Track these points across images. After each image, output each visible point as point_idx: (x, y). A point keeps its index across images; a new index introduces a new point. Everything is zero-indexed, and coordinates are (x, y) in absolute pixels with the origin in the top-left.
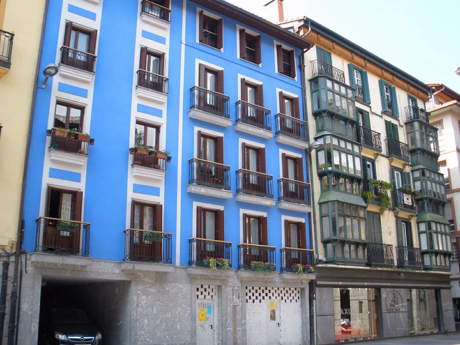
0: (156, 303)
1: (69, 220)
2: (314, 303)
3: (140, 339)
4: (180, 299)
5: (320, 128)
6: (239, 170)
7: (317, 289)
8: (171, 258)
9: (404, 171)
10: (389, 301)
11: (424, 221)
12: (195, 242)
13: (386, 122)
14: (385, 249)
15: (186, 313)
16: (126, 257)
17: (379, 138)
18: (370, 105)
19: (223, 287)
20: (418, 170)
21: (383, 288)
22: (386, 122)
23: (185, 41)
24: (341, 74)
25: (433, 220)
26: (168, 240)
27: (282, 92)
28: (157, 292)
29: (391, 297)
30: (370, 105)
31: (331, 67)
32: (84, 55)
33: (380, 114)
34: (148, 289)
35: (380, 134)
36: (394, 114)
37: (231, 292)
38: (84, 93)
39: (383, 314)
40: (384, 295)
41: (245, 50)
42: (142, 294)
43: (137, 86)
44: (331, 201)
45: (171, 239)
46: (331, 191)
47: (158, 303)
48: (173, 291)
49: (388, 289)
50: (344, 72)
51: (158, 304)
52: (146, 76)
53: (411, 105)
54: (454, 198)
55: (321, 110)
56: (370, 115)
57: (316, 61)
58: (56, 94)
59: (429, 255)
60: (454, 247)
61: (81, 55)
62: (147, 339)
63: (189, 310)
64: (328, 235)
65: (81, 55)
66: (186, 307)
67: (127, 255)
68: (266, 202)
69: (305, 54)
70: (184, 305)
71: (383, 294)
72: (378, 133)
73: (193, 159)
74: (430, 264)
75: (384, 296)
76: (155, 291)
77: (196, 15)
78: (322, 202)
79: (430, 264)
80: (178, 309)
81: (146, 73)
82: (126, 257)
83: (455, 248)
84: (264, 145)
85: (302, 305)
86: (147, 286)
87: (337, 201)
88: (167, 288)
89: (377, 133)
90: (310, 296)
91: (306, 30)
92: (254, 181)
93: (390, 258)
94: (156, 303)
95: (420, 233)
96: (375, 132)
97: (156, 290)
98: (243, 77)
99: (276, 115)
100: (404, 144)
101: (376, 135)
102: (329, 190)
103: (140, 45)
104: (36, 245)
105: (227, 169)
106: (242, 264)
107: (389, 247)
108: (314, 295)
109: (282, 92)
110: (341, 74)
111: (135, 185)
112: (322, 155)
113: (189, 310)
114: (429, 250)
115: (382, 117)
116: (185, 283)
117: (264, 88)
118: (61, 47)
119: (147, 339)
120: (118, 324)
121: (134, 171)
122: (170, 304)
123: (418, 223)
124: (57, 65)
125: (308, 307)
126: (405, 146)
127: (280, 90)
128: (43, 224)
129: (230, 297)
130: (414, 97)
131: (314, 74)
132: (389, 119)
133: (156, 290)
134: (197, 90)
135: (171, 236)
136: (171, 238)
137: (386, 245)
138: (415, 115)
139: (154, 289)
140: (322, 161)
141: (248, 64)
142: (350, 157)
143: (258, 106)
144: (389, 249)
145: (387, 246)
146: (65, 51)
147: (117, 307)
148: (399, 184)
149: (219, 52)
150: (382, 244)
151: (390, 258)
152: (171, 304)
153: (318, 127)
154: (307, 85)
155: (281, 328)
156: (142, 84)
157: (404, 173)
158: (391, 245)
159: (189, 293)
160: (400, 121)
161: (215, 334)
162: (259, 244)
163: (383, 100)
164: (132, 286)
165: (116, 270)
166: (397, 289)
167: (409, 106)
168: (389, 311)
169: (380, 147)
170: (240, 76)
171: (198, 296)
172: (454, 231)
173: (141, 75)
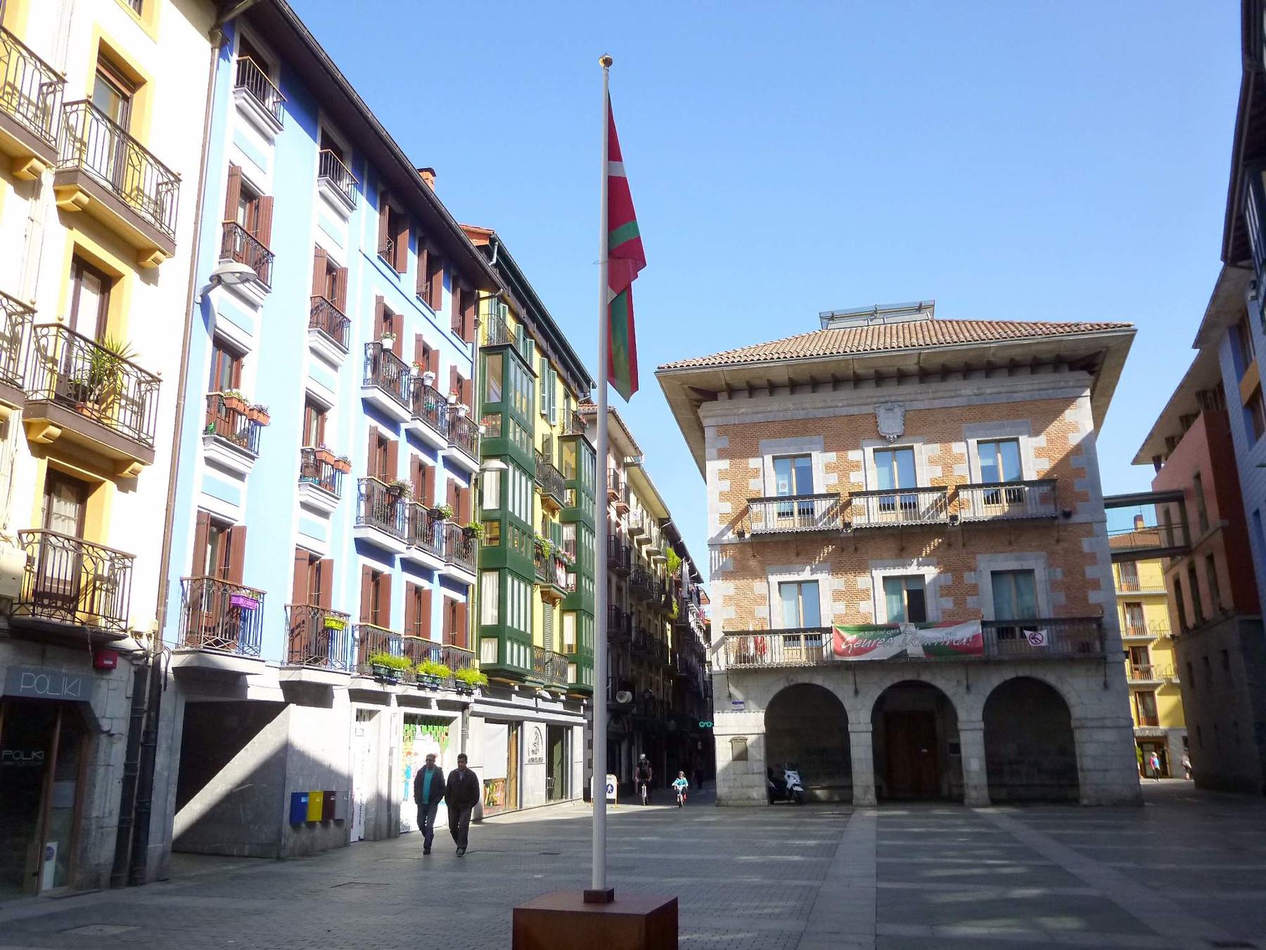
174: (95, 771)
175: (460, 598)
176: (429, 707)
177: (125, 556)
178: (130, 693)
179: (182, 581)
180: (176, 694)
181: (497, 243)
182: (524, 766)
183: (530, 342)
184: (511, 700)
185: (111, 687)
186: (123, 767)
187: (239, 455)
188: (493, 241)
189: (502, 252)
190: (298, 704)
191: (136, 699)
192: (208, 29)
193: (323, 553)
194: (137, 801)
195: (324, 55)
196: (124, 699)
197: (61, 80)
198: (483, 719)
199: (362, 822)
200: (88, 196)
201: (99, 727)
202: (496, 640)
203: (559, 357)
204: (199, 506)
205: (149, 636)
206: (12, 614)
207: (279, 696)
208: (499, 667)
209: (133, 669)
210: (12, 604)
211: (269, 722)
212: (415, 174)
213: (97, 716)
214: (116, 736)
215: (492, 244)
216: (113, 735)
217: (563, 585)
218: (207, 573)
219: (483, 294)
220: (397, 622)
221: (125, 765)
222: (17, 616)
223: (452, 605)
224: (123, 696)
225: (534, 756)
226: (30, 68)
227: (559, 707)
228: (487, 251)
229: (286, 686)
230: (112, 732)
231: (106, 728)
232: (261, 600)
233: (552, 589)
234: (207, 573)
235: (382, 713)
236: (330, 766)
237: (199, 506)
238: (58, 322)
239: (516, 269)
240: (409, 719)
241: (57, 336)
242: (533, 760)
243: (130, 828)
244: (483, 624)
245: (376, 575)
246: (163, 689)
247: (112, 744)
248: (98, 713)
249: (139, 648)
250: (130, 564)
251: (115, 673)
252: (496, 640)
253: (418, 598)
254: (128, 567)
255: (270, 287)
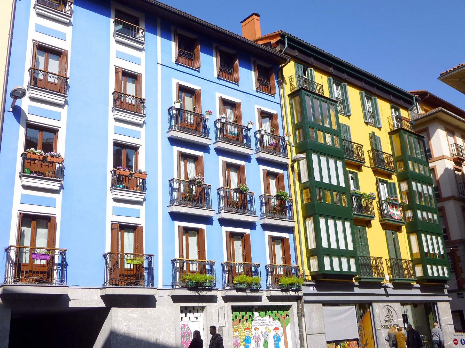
0: (138, 329)
2: (303, 321)
4: (164, 323)
6: (220, 188)
10: (383, 317)
12: (178, 262)
14: (375, 262)
15: (170, 338)
16: (106, 282)
17: (361, 150)
21: (375, 303)
23: (161, 61)
24: (320, 88)
28: (139, 317)
29: (385, 312)
32: (54, 77)
34: (129, 315)
35: (362, 145)
36: (377, 124)
37: (217, 313)
40: (376, 310)
42: (123, 320)
43: (114, 108)
45: (152, 261)
47: (140, 329)
48: (155, 315)
49: (381, 304)
50: (323, 86)
51: (140, 330)
52: (122, 97)
53: (394, 114)
54: (445, 207)
57: (294, 76)
60: (449, 257)
61: (51, 76)
63: (173, 334)
65: (51, 76)
66: (170, 331)
69: (284, 69)
70: (168, 329)
71: (376, 309)
72: (360, 145)
73: (173, 179)
75: (377, 312)
76: (137, 316)
80: (162, 334)
81: (122, 95)
82: (106, 282)
83: (450, 258)
86: (128, 311)
88: (149, 312)
89: (359, 144)
91: (283, 46)
93: (380, 271)
94: (138, 329)
96: (357, 144)
97: (138, 315)
100: (388, 154)
101: (358, 147)
103: (115, 66)
104: (5, 276)
105: (209, 187)
106: (175, 192)
107: (378, 260)
108: (303, 312)
110: (320, 88)
113: (173, 334)
116: (168, 306)
118: (29, 68)
121: (113, 194)
122: (153, 329)
124: (26, 88)
126: (389, 156)
128: (13, 253)
131: (293, 90)
133: (138, 315)
134: (177, 183)
135: (153, 258)
136: (152, 259)
137: (375, 257)
138: (399, 124)
139: (136, 314)
144: (379, 262)
145: (376, 259)
146: (34, 71)
148: (384, 195)
150: (370, 257)
151: (380, 271)
152: (154, 329)
156: (119, 105)
158: (380, 258)
159: (172, 316)
163: (365, 111)
165: (95, 297)
166: (391, 303)
167: (392, 116)
169: (364, 159)
170: (218, 95)
171: (182, 318)
172: (447, 241)
176: (260, 301)
179: (104, 256)
181: (286, 36)
182: (377, 331)
183: (310, 70)
184: (354, 291)
187: (57, 182)
188: (283, 36)
189: (291, 39)
190: (119, 307)
193: (55, 214)
195: (203, 22)
198: (399, 304)
202: (316, 257)
203: (393, 96)
204: (19, 211)
207: (102, 304)
208: (321, 273)
211: (106, 318)
212: (254, 44)
218: (119, 251)
227: (418, 292)
228: (281, 42)
229: (105, 298)
233: (386, 221)
234: (119, 251)
235: (207, 308)
236: (157, 340)
239: (362, 71)
240: (234, 309)
244: (310, 248)
252: (316, 257)
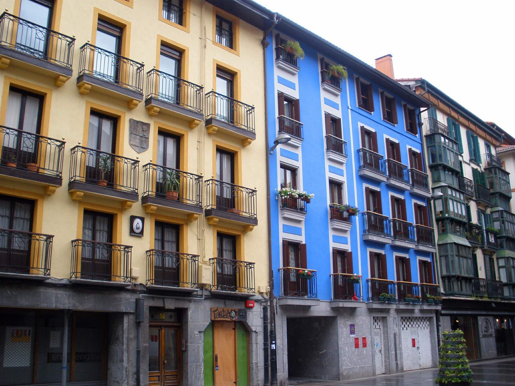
1: (175, 251)
3: (344, 364)
5: (436, 180)
7: (441, 318)
8: (316, 293)
9: (486, 213)
11: (503, 256)
13: (473, 169)
18: (462, 155)
19: (388, 318)
20: (498, 211)
22: (473, 169)
25: (511, 256)
26: (126, 254)
27: (411, 148)
30: (462, 155)
31: (436, 120)
33: (468, 162)
38: (295, 157)
39: (481, 339)
41: (361, 99)
44: (449, 243)
45: (315, 276)
46: (448, 234)
55: (437, 164)
56: (463, 163)
58: (280, 159)
59: (508, 287)
62: (348, 364)
64: (445, 273)
67: (149, 279)
68: (410, 246)
74: (509, 295)
77: (272, 39)
78: (441, 243)
79: (509, 295)
84: (379, 189)
85: (431, 332)
87: (455, 243)
90: (437, 323)
92: (346, 216)
95: (499, 268)
98: (362, 125)
99: (359, 150)
102: (447, 233)
109: (411, 148)
111: (334, 236)
112: (439, 203)
114: (509, 283)
115: (469, 164)
117: (400, 145)
119: (348, 364)
120: (320, 353)
123: (498, 259)
125: (436, 333)
127: (410, 147)
129: (392, 326)
130: (489, 144)
132: (475, 167)
140: (439, 208)
141: (409, 134)
142: (459, 205)
143: (294, 120)
147: (317, 338)
149: (415, 137)
153: (434, 178)
154: (424, 139)
155: (420, 351)
157: (487, 215)
160: (481, 167)
161: (383, 357)
162: (379, 278)
164: (338, 320)
168: (485, 336)
170: (408, 147)
173: (281, 121)
174: (252, 346)
175: (429, 260)
177: (250, 263)
178: (262, 316)
180: (282, 315)
185: (254, 314)
186: (263, 344)
191: (265, 318)
192: (259, 42)
194: (271, 357)
196: (260, 318)
197: (201, 88)
199: (384, 366)
200: (217, 127)
201: (251, 329)
205: (267, 294)
206: (211, 290)
209: (262, 307)
210: (211, 286)
213: (250, 325)
214: (258, 333)
215: (422, 84)
216: (257, 332)
217: (504, 190)
219: (422, 109)
220: (392, 275)
221: (264, 343)
222: (213, 290)
223: (423, 264)
224: (259, 317)
225: (486, 333)
226: (219, 99)
229: (333, 309)
230: (257, 331)
231: (254, 330)
232: (315, 274)
237: (283, 238)
238: (212, 178)
241: (212, 184)
242: (485, 335)
243: (268, 367)
245: (378, 255)
246: (276, 314)
247: (257, 336)
248: (250, 324)
249: (263, 298)
250: (253, 266)
251: (254, 309)
253: (403, 263)
254: (252, 268)
255: (347, 155)
